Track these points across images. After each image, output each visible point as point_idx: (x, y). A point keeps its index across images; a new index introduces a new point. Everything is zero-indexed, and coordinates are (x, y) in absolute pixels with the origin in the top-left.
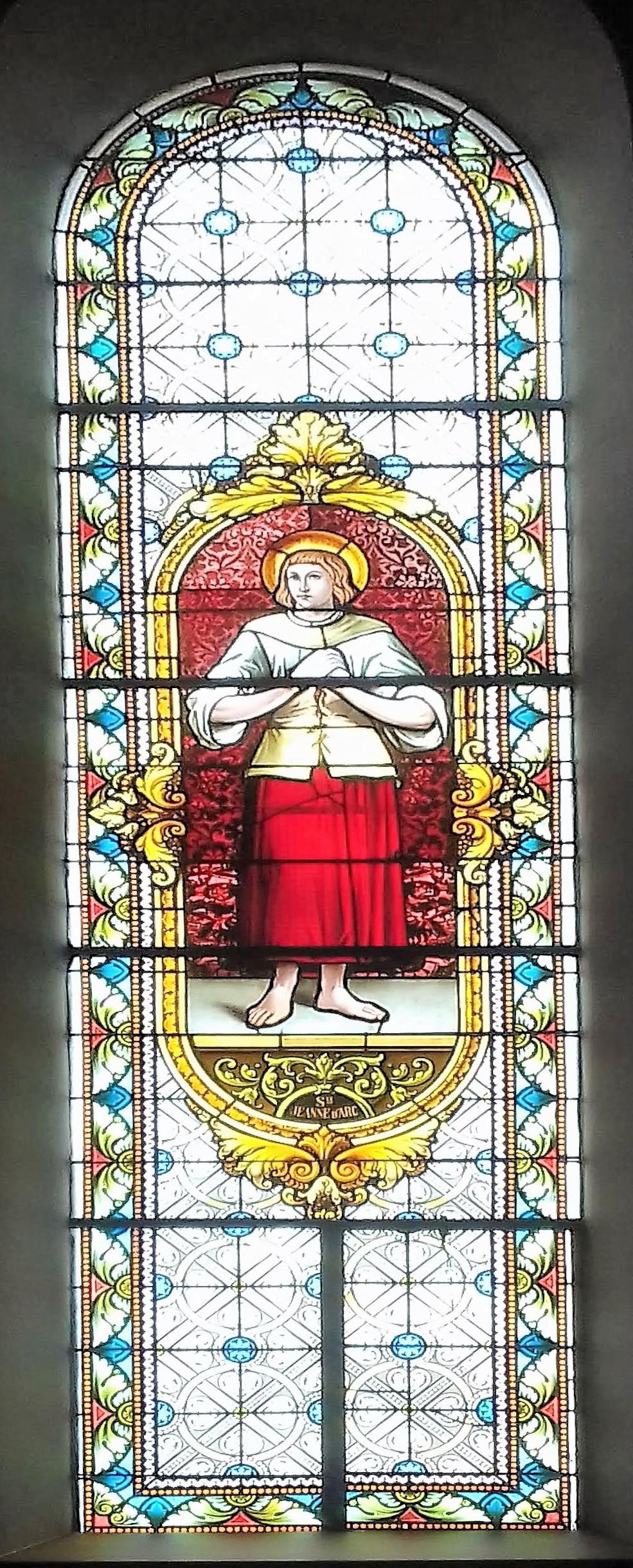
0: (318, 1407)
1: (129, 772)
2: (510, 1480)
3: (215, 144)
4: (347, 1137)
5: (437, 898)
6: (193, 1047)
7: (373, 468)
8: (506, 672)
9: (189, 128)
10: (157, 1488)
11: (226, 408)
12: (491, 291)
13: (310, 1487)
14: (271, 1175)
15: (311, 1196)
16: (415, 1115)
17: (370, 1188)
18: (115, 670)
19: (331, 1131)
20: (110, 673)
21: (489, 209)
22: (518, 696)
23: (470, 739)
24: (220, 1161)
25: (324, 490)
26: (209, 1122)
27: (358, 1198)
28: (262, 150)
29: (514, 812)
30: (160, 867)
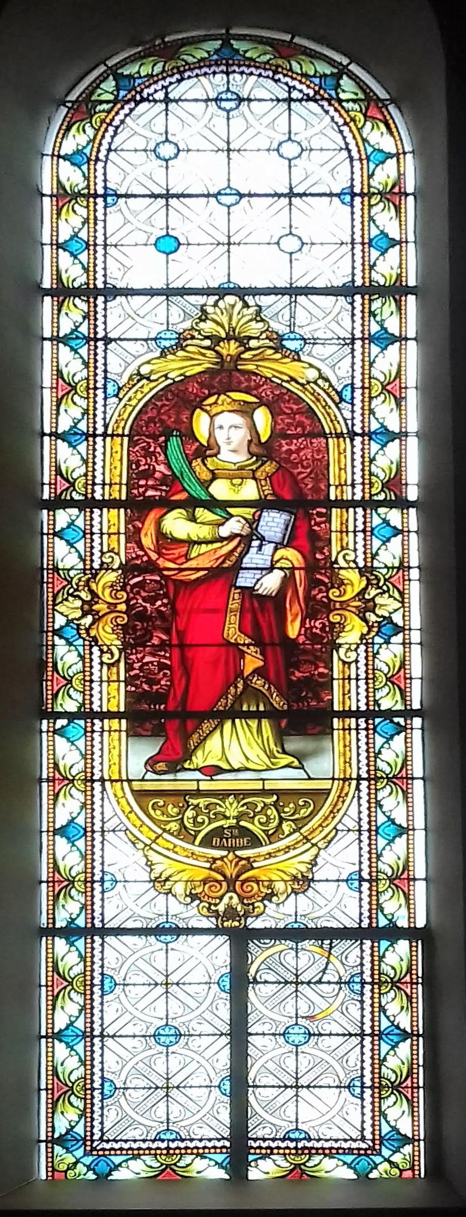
0: (228, 1083)
1: (85, 574)
2: (374, 1144)
3: (163, 87)
4: (249, 861)
5: (316, 673)
6: (132, 791)
7: (278, 343)
8: (370, 497)
9: (143, 74)
10: (103, 1150)
11: (168, 292)
12: (366, 203)
13: (222, 1148)
14: (191, 893)
15: (221, 908)
16: (301, 843)
17: (266, 902)
18: (80, 494)
19: (237, 856)
20: (76, 497)
21: (364, 140)
22: (379, 515)
23: (343, 549)
24: (151, 881)
25: (238, 357)
26: (143, 849)
27: (256, 910)
28: (199, 93)
29: (375, 605)
30: (109, 649)
